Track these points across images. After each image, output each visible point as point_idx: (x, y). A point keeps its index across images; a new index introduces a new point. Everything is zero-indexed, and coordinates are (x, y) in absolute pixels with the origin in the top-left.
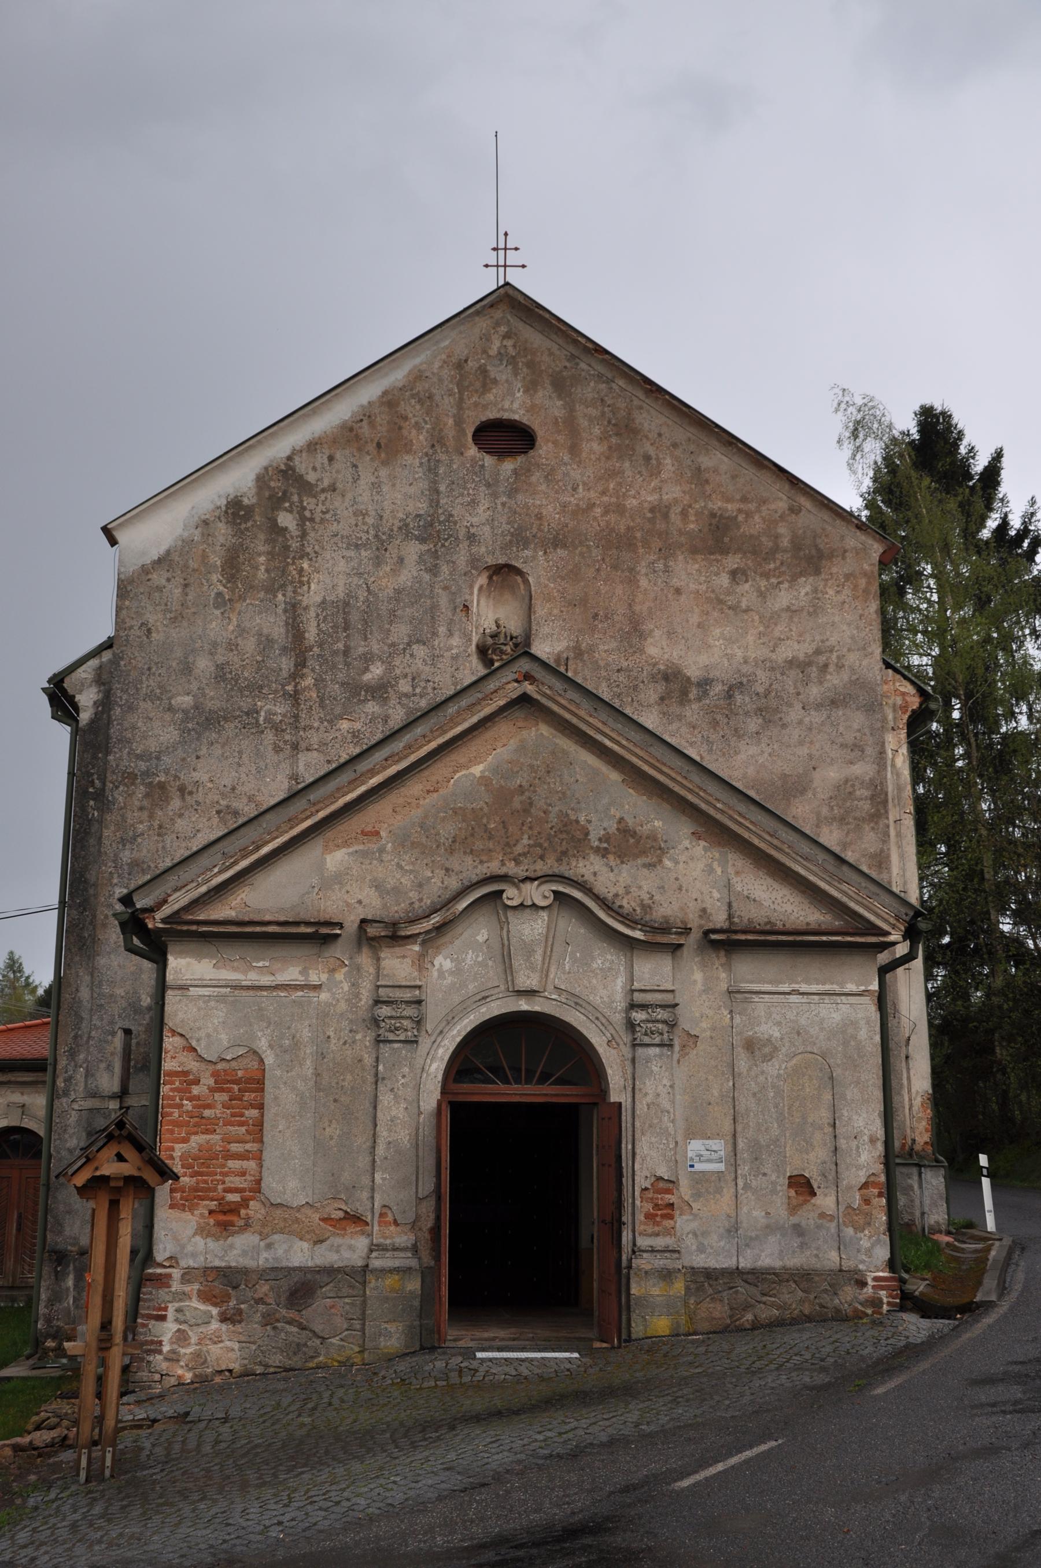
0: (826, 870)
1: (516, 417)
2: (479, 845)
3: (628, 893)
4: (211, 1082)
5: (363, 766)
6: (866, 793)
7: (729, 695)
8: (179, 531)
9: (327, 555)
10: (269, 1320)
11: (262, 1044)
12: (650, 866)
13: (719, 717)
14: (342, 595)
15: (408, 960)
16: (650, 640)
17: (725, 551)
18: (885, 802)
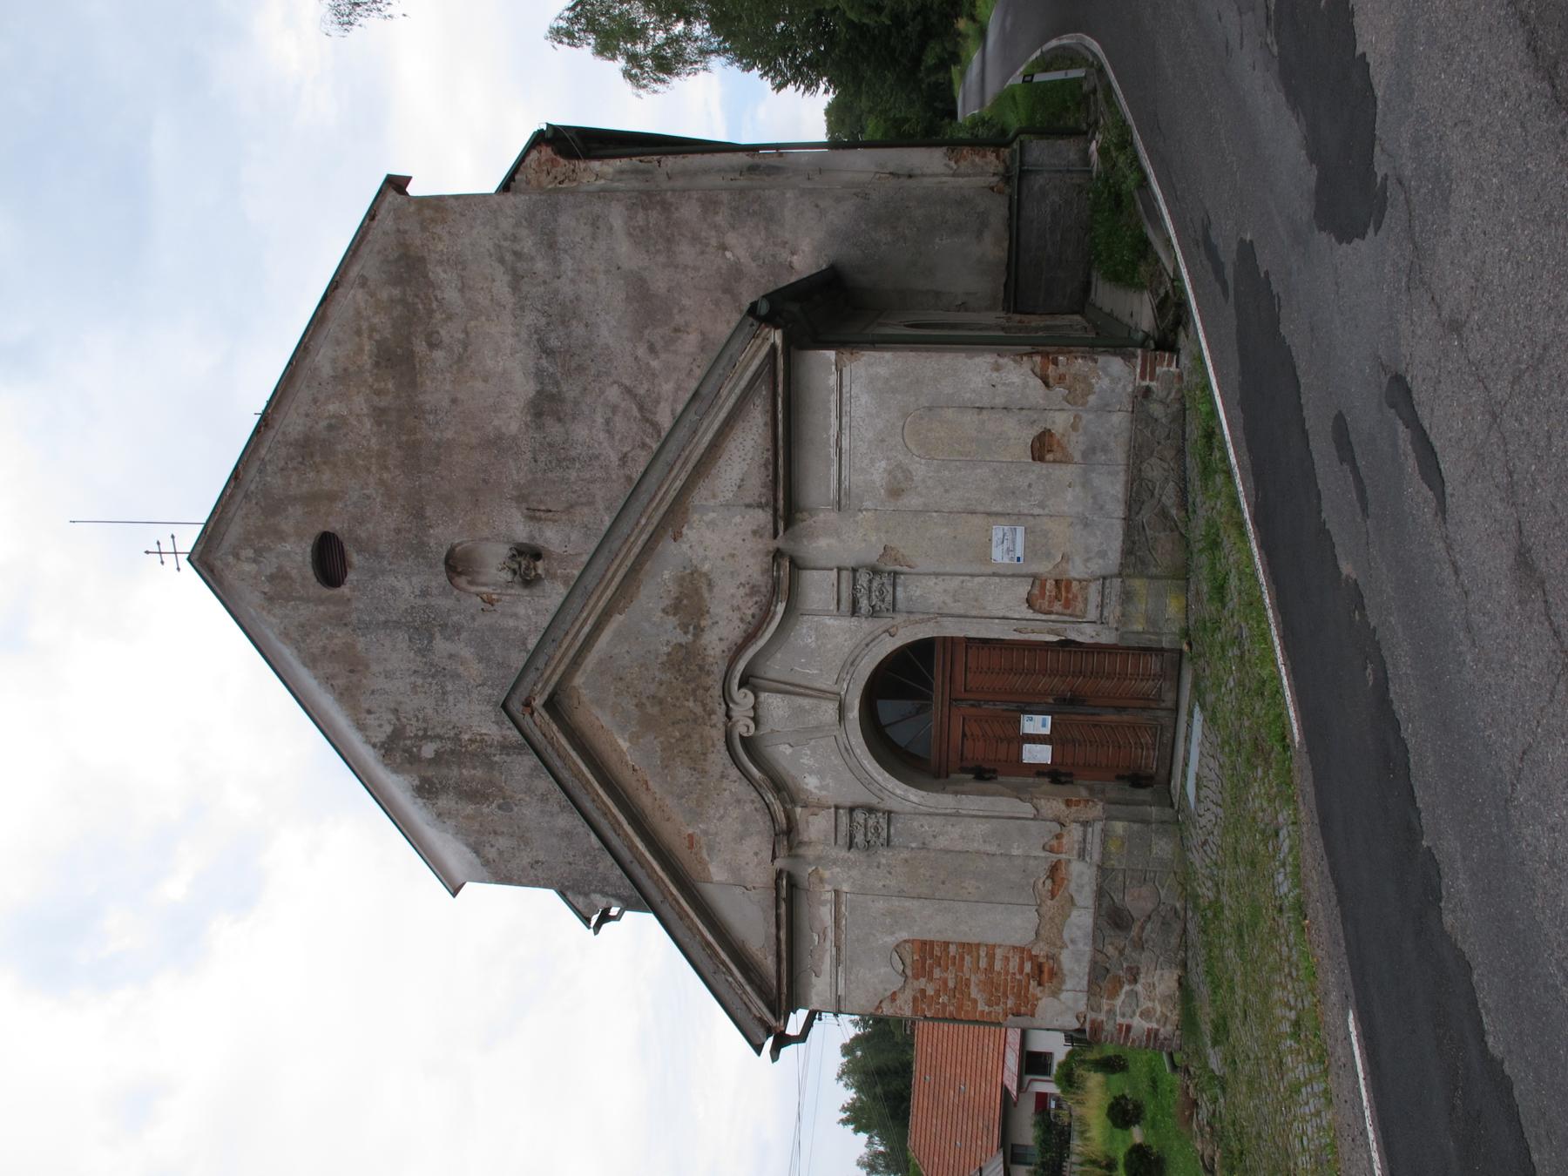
0: (706, 413)
1: (309, 549)
2: (697, 747)
3: (739, 608)
4: (923, 980)
5: (626, 854)
6: (641, 215)
7: (548, 352)
8: (449, 836)
9: (455, 719)
10: (1140, 945)
11: (890, 940)
12: (710, 585)
13: (573, 365)
14: (489, 708)
15: (811, 818)
16: (504, 430)
17: (410, 356)
18: (649, 194)
